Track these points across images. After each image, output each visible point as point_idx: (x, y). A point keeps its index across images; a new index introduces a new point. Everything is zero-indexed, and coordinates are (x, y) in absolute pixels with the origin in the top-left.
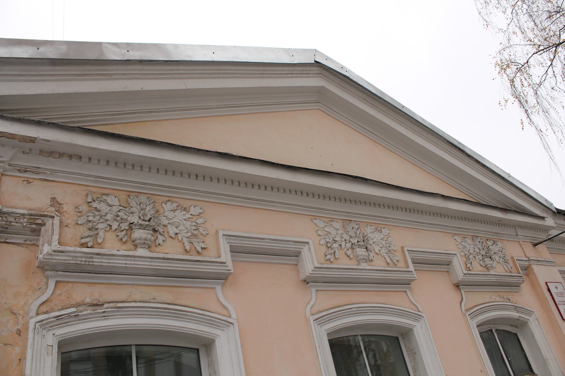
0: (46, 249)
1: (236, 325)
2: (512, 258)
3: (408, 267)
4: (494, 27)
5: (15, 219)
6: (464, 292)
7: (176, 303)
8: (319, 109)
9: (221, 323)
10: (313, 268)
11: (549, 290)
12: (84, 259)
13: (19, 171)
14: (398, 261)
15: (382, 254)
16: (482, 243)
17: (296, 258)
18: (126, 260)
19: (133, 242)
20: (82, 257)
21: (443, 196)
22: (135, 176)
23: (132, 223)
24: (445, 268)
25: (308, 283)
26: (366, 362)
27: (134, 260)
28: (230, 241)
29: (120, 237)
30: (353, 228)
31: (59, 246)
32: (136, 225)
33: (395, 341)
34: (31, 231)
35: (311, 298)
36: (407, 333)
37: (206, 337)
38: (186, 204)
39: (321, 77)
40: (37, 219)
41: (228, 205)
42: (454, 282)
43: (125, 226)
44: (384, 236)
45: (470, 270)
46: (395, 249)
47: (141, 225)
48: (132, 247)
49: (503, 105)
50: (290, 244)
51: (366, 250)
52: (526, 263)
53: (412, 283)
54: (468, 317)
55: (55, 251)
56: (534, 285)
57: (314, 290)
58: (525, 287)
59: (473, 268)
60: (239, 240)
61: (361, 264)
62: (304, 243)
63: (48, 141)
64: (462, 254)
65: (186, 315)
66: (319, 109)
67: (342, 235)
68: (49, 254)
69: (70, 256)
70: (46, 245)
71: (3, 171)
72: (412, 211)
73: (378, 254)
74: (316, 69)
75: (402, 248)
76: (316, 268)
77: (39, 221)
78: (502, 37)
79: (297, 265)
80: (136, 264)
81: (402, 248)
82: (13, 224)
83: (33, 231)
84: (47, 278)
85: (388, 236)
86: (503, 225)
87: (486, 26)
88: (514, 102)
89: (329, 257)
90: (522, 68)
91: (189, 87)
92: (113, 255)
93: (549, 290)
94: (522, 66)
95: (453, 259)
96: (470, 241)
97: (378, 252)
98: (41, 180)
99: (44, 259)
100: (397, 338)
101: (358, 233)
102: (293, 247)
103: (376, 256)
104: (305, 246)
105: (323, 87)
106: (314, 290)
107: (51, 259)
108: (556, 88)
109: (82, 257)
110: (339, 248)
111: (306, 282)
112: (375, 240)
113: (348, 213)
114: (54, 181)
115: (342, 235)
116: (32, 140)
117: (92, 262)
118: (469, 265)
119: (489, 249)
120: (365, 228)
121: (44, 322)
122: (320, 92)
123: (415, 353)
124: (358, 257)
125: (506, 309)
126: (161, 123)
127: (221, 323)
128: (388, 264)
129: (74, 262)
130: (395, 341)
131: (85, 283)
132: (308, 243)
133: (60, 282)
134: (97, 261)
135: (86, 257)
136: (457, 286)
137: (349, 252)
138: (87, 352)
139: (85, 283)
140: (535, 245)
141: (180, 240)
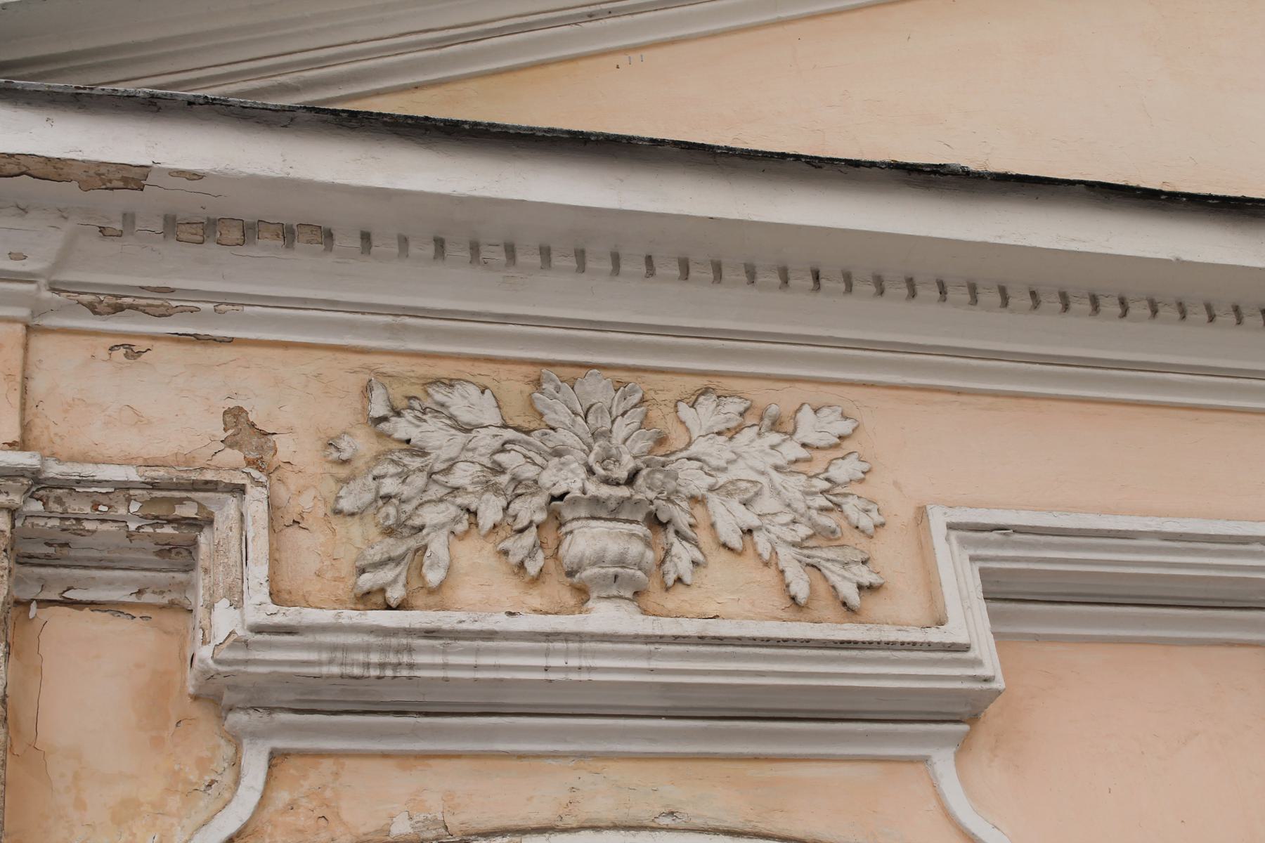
0: (225, 621)
5: (95, 507)
12: (375, 658)
13: (93, 309)
18: (547, 653)
19: (570, 574)
20: (367, 649)
23: (561, 497)
27: (581, 653)
29: (514, 559)
31: (273, 608)
32: (575, 501)
34: (159, 553)
38: (780, 400)
40: (181, 501)
43: (530, 509)
44: (803, 453)
47: (596, 501)
48: (569, 599)
55: (259, 629)
69: (320, 647)
70: (222, 605)
71: (33, 314)
77: (188, 511)
80: (590, 669)
82: (89, 526)
83: (167, 550)
84: (235, 740)
92: (490, 635)
98: (179, 338)
107: (247, 662)
109: (367, 649)
114: (230, 341)
117: (411, 666)
129: (335, 670)
131: (385, 755)
135: (385, 649)
139: (385, 755)
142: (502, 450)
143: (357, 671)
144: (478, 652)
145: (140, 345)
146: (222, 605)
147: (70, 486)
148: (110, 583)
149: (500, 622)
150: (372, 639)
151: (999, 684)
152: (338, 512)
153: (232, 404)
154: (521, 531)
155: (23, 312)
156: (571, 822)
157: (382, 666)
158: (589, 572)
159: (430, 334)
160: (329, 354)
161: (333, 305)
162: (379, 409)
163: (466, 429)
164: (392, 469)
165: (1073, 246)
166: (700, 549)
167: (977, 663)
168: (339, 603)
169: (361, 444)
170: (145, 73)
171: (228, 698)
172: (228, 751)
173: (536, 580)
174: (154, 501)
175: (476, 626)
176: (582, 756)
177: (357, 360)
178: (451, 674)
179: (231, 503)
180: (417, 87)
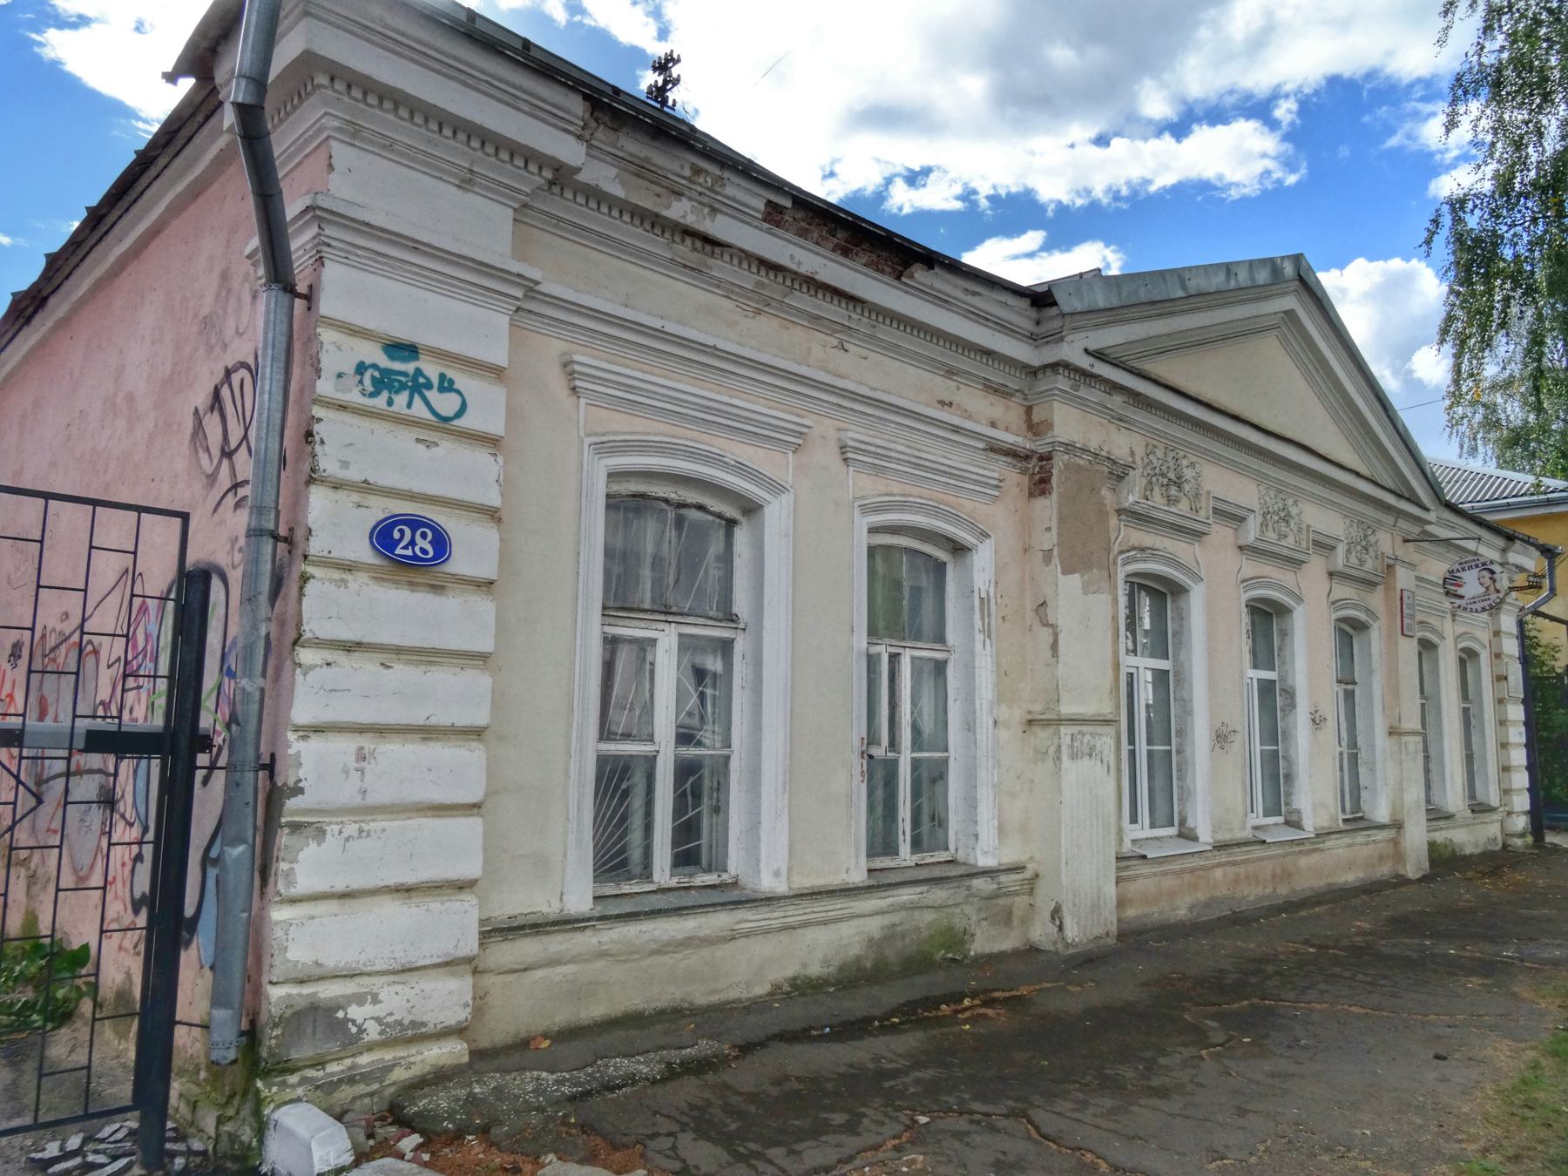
0: (1131, 499)
1: (792, 491)
11: (1401, 599)
26: (1484, 691)
43: (1165, 481)
52: (1391, 562)
56: (1389, 588)
58: (1380, 588)
93: (1401, 599)
94: (61, 887)
96: (1272, 494)
111: (1241, 548)
119: (446, 386)
121: (438, 175)
125: (673, 455)
134: (1154, 514)
136: (1331, 574)
138: (879, 587)
140: (1406, 541)
141: (225, 462)
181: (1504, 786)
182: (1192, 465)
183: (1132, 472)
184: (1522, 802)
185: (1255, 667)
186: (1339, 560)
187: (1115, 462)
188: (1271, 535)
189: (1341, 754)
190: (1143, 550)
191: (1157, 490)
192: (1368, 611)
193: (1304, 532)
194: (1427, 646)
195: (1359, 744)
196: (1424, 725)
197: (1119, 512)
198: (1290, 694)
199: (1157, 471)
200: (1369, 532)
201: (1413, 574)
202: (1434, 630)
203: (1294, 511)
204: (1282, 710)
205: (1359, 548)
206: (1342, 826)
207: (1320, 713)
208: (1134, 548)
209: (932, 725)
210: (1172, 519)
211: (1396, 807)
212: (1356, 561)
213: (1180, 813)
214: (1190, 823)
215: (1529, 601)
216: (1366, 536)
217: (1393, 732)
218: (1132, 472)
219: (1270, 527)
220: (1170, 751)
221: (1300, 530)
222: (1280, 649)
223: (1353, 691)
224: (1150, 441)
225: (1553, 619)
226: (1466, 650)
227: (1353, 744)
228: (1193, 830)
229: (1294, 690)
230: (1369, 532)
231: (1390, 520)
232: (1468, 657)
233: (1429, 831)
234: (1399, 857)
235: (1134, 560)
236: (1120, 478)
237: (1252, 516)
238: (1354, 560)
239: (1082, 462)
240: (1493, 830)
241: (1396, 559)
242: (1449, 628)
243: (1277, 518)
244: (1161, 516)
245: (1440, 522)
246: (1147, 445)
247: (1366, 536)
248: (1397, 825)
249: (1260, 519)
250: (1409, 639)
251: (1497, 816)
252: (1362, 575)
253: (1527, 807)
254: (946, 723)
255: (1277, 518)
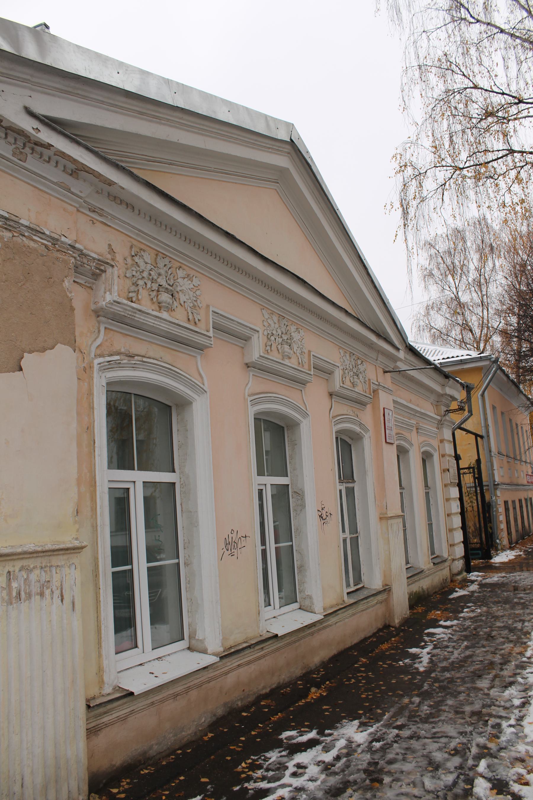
0: (108, 298)
2: (309, 352)
3: (310, 370)
4: (410, 115)
5: (88, 262)
6: (106, 328)
7: (174, 364)
8: (276, 190)
9: (199, 390)
10: (258, 356)
12: (130, 313)
13: (90, 210)
14: (199, 320)
15: (186, 306)
16: (287, 326)
17: (244, 341)
18: (155, 320)
19: (159, 303)
20: (129, 311)
21: (346, 312)
22: (164, 237)
23: (161, 286)
24: (326, 376)
25: (248, 367)
27: (160, 322)
28: (215, 318)
29: (151, 297)
30: (165, 265)
31: (118, 297)
32: (163, 287)
33: (167, 409)
34: (92, 275)
35: (249, 381)
36: (293, 425)
37: (186, 399)
38: (192, 273)
39: (289, 157)
40: (102, 265)
41: (214, 280)
42: (330, 391)
43: (155, 286)
44: (193, 287)
45: (132, 302)
46: (200, 306)
47: (167, 289)
48: (158, 309)
49: (388, 209)
50: (247, 330)
51: (171, 296)
52: (376, 387)
53: (308, 385)
54: (249, 403)
55: (115, 301)
56: (375, 408)
57: (251, 374)
59: (271, 350)
60: (220, 318)
61: (286, 360)
62: (255, 330)
63: (123, 189)
64: (266, 333)
65: (180, 378)
66: (276, 190)
67: (151, 272)
68: (110, 303)
69: (122, 308)
70: (108, 293)
71: (80, 207)
72: (188, 241)
73: (295, 353)
74: (288, 148)
75: (208, 306)
76: (260, 356)
77: (102, 268)
78: (412, 131)
79: (243, 348)
80: (160, 325)
81: (309, 352)
82: (85, 265)
83: (94, 274)
84: (99, 322)
85: (197, 287)
86: (257, 279)
87: (402, 109)
88: (397, 209)
89: (131, 295)
90: (420, 176)
91: (207, 148)
92: (148, 314)
95: (253, 336)
96: (275, 318)
97: (183, 304)
98: (102, 222)
99: (106, 306)
100: (283, 428)
101: (169, 273)
102: (247, 332)
103: (179, 306)
104: (255, 333)
105: (288, 169)
106: (251, 374)
107: (111, 308)
108: (438, 210)
109: (129, 311)
110: (144, 287)
111: (248, 366)
112: (183, 288)
113: (283, 309)
114: (110, 226)
115: (151, 272)
116: (111, 183)
117: (135, 316)
118: (268, 348)
120: (177, 269)
122: (282, 172)
123: (296, 445)
124: (284, 353)
126: (418, 347)
127: (199, 390)
128: (299, 364)
129: (123, 314)
130: (167, 409)
131: (121, 333)
132: (258, 332)
133: (109, 329)
134: (139, 317)
135: (132, 312)
136: (331, 395)
137: (279, 347)
139: (121, 333)
140: (385, 372)
142: (150, 270)
143: (126, 315)
144: (145, 317)
145: (95, 221)
146: (108, 293)
147: (86, 255)
148: (82, 279)
149: (150, 311)
150: (131, 309)
151: (212, 346)
152: (126, 276)
153: (109, 243)
154: (153, 291)
155: (77, 206)
156: (147, 356)
157: (130, 315)
158: (164, 304)
159: (143, 238)
160: (124, 235)
161: (128, 224)
162: (133, 254)
163: (146, 263)
164: (135, 269)
165: (244, 259)
166: (461, 384)
167: (211, 341)
168: (124, 298)
169: (129, 260)
170: (104, 147)
171: (101, 313)
172: (97, 325)
173: (154, 303)
174: (98, 264)
175: (147, 311)
176: (149, 342)
177: (129, 239)
178: (140, 320)
179: (111, 268)
180: (140, 169)
181: (450, 542)
182: (188, 277)
183: (109, 270)
184: (460, 551)
185: (260, 473)
186: (337, 384)
187: (82, 254)
188: (275, 356)
189: (345, 541)
190: (131, 356)
191: (144, 294)
192: (361, 425)
193: (306, 356)
194: (402, 452)
195: (359, 530)
196: (403, 511)
197: (98, 313)
198: (300, 495)
199: (145, 274)
200: (359, 362)
201: (391, 398)
202: (405, 440)
203: (296, 336)
204: (295, 510)
205: (352, 373)
206: (349, 601)
207: (326, 509)
208: (119, 353)
209: (515, 536)
210: (164, 326)
211: (387, 575)
212: (349, 384)
213: (190, 625)
214: (199, 635)
215: (457, 418)
216: (356, 365)
217: (384, 518)
218: (109, 270)
219: (274, 347)
220: (178, 564)
221: (302, 353)
222: (291, 458)
223: (353, 488)
224: (135, 242)
225: (468, 431)
226: (424, 453)
227: (354, 529)
228: (202, 641)
229: (303, 492)
230: (359, 362)
231: (373, 355)
232: (426, 458)
233: (408, 585)
234: (389, 612)
235: (119, 365)
236: (96, 276)
237: (256, 336)
238: (348, 385)
239: (32, 244)
240: (445, 573)
241: (379, 385)
242: (414, 437)
243: (280, 340)
244: (151, 321)
245: (405, 362)
246: (131, 247)
247: (356, 365)
248: (387, 590)
249: (263, 339)
250: (389, 446)
251: (447, 564)
252: (354, 395)
253: (463, 554)
254: (416, 538)
255: (280, 340)
